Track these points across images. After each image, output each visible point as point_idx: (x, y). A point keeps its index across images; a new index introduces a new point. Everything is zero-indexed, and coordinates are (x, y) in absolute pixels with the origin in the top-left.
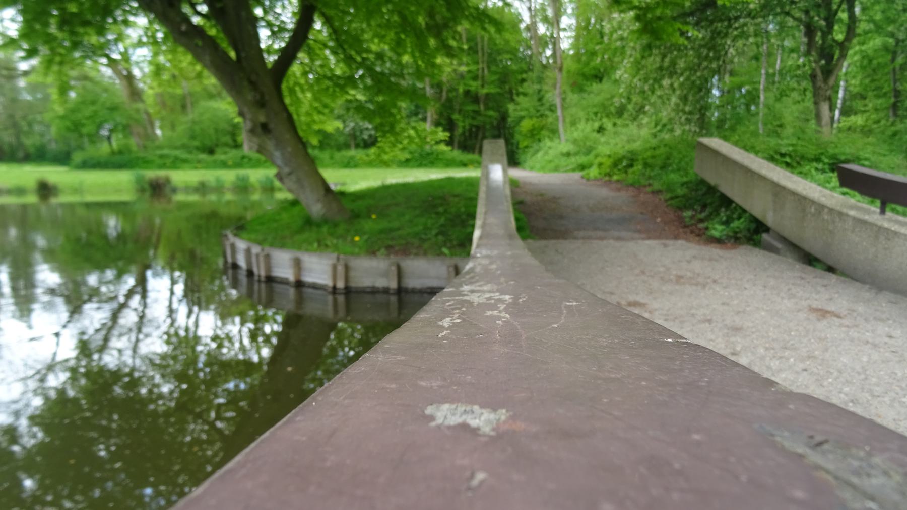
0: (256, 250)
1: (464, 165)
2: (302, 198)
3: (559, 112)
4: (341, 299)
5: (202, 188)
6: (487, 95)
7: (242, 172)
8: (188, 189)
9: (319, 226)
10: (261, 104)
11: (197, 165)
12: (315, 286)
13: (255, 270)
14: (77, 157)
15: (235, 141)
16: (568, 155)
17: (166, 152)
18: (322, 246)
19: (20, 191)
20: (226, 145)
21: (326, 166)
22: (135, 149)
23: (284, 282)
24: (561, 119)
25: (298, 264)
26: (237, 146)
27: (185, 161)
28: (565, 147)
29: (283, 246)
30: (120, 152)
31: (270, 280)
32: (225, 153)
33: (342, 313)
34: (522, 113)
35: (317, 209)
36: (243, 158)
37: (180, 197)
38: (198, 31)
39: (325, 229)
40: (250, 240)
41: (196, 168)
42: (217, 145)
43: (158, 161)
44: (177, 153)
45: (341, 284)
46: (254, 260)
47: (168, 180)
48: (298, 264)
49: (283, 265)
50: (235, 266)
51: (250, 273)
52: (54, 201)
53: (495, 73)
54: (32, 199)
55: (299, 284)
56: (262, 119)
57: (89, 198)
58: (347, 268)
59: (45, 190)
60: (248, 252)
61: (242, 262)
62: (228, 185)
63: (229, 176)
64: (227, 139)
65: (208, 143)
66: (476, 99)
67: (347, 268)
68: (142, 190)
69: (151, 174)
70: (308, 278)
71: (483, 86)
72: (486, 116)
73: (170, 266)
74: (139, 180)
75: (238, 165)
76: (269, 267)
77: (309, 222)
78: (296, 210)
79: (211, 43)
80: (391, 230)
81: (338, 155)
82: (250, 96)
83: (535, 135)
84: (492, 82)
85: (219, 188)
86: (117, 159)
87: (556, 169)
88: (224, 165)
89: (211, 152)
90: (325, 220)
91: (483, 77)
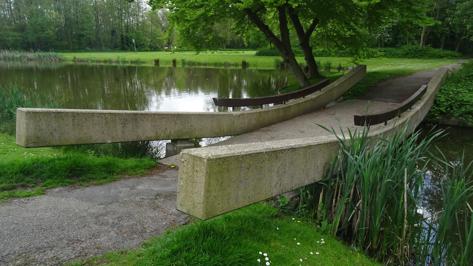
19: (237, 65)
54: (240, 67)
56: (287, 59)
68: (277, 66)
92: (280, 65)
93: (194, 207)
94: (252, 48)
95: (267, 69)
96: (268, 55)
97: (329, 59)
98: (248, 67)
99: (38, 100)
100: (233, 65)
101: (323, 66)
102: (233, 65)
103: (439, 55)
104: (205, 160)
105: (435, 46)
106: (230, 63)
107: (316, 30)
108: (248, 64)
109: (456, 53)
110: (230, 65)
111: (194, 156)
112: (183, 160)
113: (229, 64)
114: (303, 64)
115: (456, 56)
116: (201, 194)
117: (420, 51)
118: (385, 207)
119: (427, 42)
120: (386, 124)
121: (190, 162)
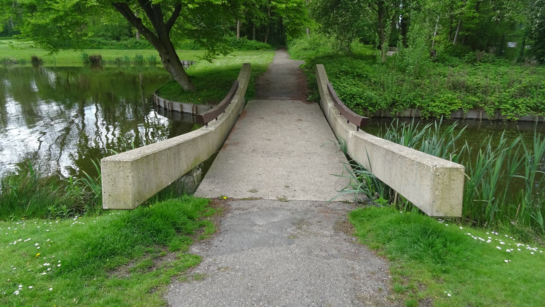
0: (167, 102)
4: (195, 117)
5: (118, 61)
8: (110, 62)
12: (187, 113)
13: (167, 108)
15: (131, 33)
16: (305, 49)
18: (189, 101)
19: (23, 62)
20: (127, 35)
23: (178, 112)
25: (181, 106)
26: (132, 36)
27: (104, 44)
28: (307, 45)
29: (176, 101)
31: (173, 111)
32: (126, 40)
33: (195, 121)
36: (136, 43)
37: (107, 66)
39: (189, 95)
40: (164, 98)
41: (111, 48)
45: (195, 113)
46: (167, 105)
47: (100, 57)
48: (181, 106)
49: (177, 106)
50: (159, 106)
51: (165, 109)
54: (30, 65)
55: (182, 113)
56: (168, 58)
57: (58, 65)
58: (197, 108)
60: (165, 102)
61: (162, 105)
62: (131, 60)
63: (132, 54)
65: (116, 33)
67: (197, 108)
68: (87, 62)
69: (91, 53)
70: (175, 109)
73: (96, 101)
74: (85, 56)
75: (134, 47)
76: (172, 107)
77: (183, 91)
79: (152, 34)
80: (210, 96)
85: (127, 62)
87: (298, 57)
88: (126, 47)
89: (118, 39)
90: (189, 91)
92: (89, 60)
93: (452, 208)
95: (70, 65)
97: (140, 52)
98: (42, 64)
101: (147, 61)
103: (256, 47)
105: (250, 38)
106: (12, 59)
108: (41, 60)
109: (268, 45)
110: (12, 62)
111: (450, 168)
112: (437, 174)
113: (11, 61)
115: (268, 48)
116: (459, 197)
117: (238, 43)
119: (242, 35)
120: (217, 119)
121: (446, 174)
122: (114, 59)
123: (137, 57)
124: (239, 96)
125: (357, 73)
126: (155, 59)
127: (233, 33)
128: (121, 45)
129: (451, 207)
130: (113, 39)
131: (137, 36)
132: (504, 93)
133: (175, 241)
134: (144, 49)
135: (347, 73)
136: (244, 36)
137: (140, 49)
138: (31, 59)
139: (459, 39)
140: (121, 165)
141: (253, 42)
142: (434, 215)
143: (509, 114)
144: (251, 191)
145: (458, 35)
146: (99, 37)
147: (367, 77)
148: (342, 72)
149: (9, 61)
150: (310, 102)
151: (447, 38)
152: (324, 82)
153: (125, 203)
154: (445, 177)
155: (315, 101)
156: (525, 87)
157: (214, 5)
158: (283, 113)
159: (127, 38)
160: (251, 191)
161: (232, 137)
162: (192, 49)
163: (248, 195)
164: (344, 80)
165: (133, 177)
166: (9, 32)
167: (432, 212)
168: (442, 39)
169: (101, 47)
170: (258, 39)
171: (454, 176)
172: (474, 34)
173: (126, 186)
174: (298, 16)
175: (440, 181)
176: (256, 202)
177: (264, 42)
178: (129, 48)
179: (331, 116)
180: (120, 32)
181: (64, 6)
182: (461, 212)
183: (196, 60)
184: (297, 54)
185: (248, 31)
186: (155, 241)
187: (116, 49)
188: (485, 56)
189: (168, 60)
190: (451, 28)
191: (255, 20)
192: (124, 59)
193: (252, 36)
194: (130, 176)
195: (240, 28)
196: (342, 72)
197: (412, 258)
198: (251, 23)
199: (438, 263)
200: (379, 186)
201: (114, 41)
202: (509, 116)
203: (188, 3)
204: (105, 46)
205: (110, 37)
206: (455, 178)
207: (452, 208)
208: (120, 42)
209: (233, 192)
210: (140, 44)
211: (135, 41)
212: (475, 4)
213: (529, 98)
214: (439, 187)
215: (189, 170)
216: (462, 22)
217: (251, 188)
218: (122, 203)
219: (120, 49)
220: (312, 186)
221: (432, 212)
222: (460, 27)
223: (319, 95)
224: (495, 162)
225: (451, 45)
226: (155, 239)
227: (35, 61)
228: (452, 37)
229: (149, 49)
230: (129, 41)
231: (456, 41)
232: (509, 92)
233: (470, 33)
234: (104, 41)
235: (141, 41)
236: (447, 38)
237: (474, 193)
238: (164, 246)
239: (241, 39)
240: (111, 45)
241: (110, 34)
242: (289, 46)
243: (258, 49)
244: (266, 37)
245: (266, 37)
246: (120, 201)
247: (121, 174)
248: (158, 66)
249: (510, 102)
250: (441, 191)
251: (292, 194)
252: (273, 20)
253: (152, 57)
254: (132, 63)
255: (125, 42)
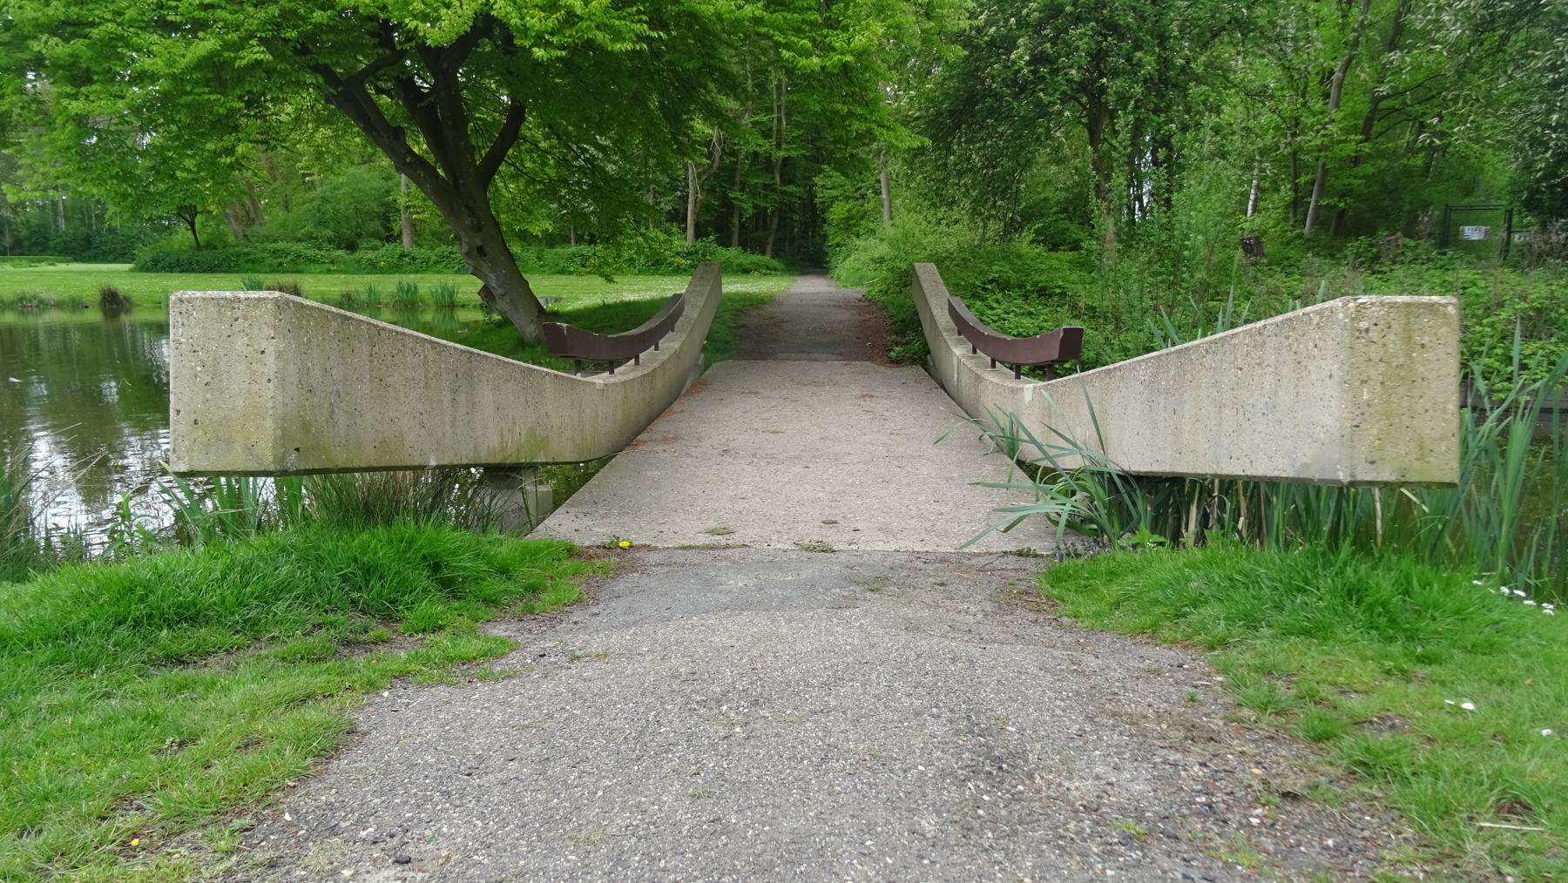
1: (745, 271)
2: (515, 318)
3: (884, 196)
6: (786, 160)
7: (409, 279)
9: (532, 346)
10: (478, 228)
11: (332, 267)
14: (144, 254)
15: (390, 230)
17: (280, 245)
19: (76, 305)
20: (376, 235)
21: (532, 271)
22: (231, 239)
24: (886, 204)
30: (210, 245)
32: (375, 248)
34: (834, 193)
35: (530, 330)
38: (419, 161)
41: (329, 271)
42: (359, 236)
43: (270, 260)
44: (299, 247)
52: (125, 319)
53: (798, 125)
54: (94, 316)
56: (479, 243)
59: (113, 302)
62: (385, 299)
64: (376, 225)
66: (768, 166)
71: (778, 146)
72: (784, 192)
75: (395, 268)
78: (506, 331)
81: (549, 254)
82: (468, 221)
83: (850, 225)
84: (794, 141)
86: (207, 255)
88: (373, 268)
89: (352, 247)
91: (779, 131)
93: (1424, 450)
94: (60, 253)
96: (193, 271)
98: (128, 311)
99: (140, 78)
100: (60, 305)
102: (60, 305)
103: (740, 265)
104: (1450, 308)
105: (725, 242)
106: (44, 296)
107: (525, 139)
108: (127, 299)
109: (775, 263)
110: (44, 305)
112: (1363, 325)
113: (41, 301)
114: (354, 296)
116: (1444, 411)
118: (1500, 420)
119: (700, 233)
121: (1395, 325)
122: (337, 297)
123: (401, 289)
124: (684, 336)
125: (1035, 284)
126: (451, 295)
127: (675, 229)
128: (358, 262)
129: (1421, 447)
130: (339, 248)
131: (406, 239)
132: (1478, 328)
133: (433, 607)
134: (424, 271)
135: (1004, 286)
136: (707, 236)
137: (411, 272)
138: (98, 298)
139: (1319, 222)
140: (238, 314)
141: (733, 253)
142: (1361, 477)
143: (1499, 386)
144: (713, 532)
145: (1318, 207)
146: (299, 240)
147: (1063, 294)
148: (991, 282)
149: (35, 303)
150: (897, 362)
151: (1286, 220)
152: (938, 301)
153: (249, 449)
154: (1392, 337)
155: (914, 362)
156: (1538, 311)
157: (612, 53)
158: (815, 383)
159: (378, 243)
160: (713, 532)
161: (661, 427)
162: (562, 272)
163: (703, 540)
164: (997, 301)
165: (279, 355)
166: (51, 244)
167: (1353, 467)
168: (1272, 222)
169: (301, 267)
170: (745, 244)
171: (1423, 332)
172: (1364, 207)
173: (256, 387)
174: (859, 111)
175: (1375, 352)
176: (729, 552)
177: (763, 253)
178: (382, 271)
179: (966, 379)
180: (358, 226)
181: (170, 63)
182: (1455, 464)
183: (572, 292)
184: (859, 274)
185: (719, 224)
186: (354, 602)
187: (345, 272)
188: (1405, 246)
189: (480, 250)
190: (1296, 191)
191: (738, 194)
192: (364, 297)
193: (730, 238)
194: (270, 350)
195: (697, 215)
196: (991, 282)
197: (1287, 632)
198: (728, 205)
199: (1391, 640)
200: (1134, 503)
201: (339, 252)
202: (1499, 391)
203: (533, 46)
204: (312, 267)
205: (330, 241)
206: (1426, 340)
207: (1424, 450)
208: (357, 255)
209: (654, 533)
210: (414, 259)
211: (399, 250)
212: (1361, 122)
213: (1553, 339)
214: (1372, 373)
215: (512, 460)
216: (1325, 172)
217: (712, 525)
218: (238, 449)
219: (357, 271)
220: (913, 522)
221: (1353, 467)
222: (1322, 186)
223: (926, 344)
224: (1505, 433)
225: (1300, 236)
226: (355, 595)
227: (111, 302)
228: (1300, 217)
229: (439, 272)
230: (382, 251)
231: (1312, 225)
232: (1492, 325)
233: (1349, 201)
234: (310, 253)
235: (416, 251)
236: (1286, 220)
237: (1502, 396)
238: (388, 618)
239: (699, 245)
240: (332, 262)
241: (329, 233)
242: (833, 263)
243: (746, 271)
244: (771, 240)
245: (771, 240)
246: (230, 442)
247: (240, 343)
248: (462, 316)
249: (1499, 351)
250: (1378, 388)
251: (847, 537)
252: (791, 194)
253: (444, 289)
254: (386, 305)
255: (371, 255)
